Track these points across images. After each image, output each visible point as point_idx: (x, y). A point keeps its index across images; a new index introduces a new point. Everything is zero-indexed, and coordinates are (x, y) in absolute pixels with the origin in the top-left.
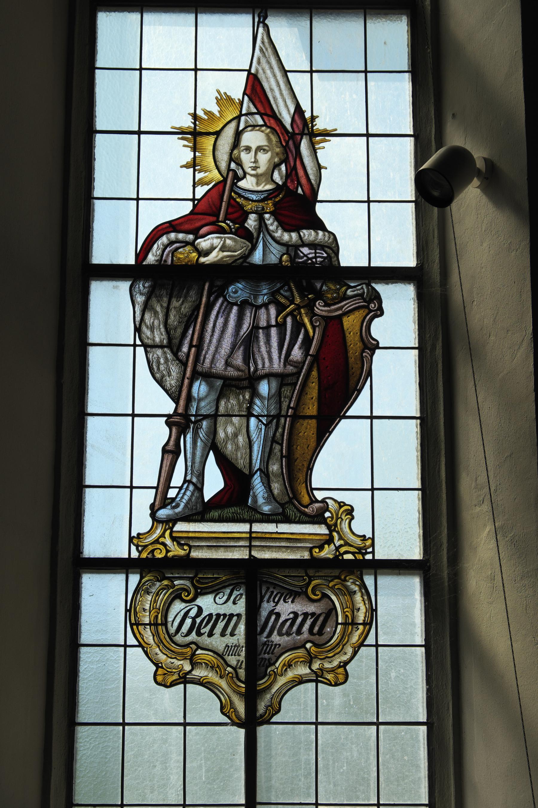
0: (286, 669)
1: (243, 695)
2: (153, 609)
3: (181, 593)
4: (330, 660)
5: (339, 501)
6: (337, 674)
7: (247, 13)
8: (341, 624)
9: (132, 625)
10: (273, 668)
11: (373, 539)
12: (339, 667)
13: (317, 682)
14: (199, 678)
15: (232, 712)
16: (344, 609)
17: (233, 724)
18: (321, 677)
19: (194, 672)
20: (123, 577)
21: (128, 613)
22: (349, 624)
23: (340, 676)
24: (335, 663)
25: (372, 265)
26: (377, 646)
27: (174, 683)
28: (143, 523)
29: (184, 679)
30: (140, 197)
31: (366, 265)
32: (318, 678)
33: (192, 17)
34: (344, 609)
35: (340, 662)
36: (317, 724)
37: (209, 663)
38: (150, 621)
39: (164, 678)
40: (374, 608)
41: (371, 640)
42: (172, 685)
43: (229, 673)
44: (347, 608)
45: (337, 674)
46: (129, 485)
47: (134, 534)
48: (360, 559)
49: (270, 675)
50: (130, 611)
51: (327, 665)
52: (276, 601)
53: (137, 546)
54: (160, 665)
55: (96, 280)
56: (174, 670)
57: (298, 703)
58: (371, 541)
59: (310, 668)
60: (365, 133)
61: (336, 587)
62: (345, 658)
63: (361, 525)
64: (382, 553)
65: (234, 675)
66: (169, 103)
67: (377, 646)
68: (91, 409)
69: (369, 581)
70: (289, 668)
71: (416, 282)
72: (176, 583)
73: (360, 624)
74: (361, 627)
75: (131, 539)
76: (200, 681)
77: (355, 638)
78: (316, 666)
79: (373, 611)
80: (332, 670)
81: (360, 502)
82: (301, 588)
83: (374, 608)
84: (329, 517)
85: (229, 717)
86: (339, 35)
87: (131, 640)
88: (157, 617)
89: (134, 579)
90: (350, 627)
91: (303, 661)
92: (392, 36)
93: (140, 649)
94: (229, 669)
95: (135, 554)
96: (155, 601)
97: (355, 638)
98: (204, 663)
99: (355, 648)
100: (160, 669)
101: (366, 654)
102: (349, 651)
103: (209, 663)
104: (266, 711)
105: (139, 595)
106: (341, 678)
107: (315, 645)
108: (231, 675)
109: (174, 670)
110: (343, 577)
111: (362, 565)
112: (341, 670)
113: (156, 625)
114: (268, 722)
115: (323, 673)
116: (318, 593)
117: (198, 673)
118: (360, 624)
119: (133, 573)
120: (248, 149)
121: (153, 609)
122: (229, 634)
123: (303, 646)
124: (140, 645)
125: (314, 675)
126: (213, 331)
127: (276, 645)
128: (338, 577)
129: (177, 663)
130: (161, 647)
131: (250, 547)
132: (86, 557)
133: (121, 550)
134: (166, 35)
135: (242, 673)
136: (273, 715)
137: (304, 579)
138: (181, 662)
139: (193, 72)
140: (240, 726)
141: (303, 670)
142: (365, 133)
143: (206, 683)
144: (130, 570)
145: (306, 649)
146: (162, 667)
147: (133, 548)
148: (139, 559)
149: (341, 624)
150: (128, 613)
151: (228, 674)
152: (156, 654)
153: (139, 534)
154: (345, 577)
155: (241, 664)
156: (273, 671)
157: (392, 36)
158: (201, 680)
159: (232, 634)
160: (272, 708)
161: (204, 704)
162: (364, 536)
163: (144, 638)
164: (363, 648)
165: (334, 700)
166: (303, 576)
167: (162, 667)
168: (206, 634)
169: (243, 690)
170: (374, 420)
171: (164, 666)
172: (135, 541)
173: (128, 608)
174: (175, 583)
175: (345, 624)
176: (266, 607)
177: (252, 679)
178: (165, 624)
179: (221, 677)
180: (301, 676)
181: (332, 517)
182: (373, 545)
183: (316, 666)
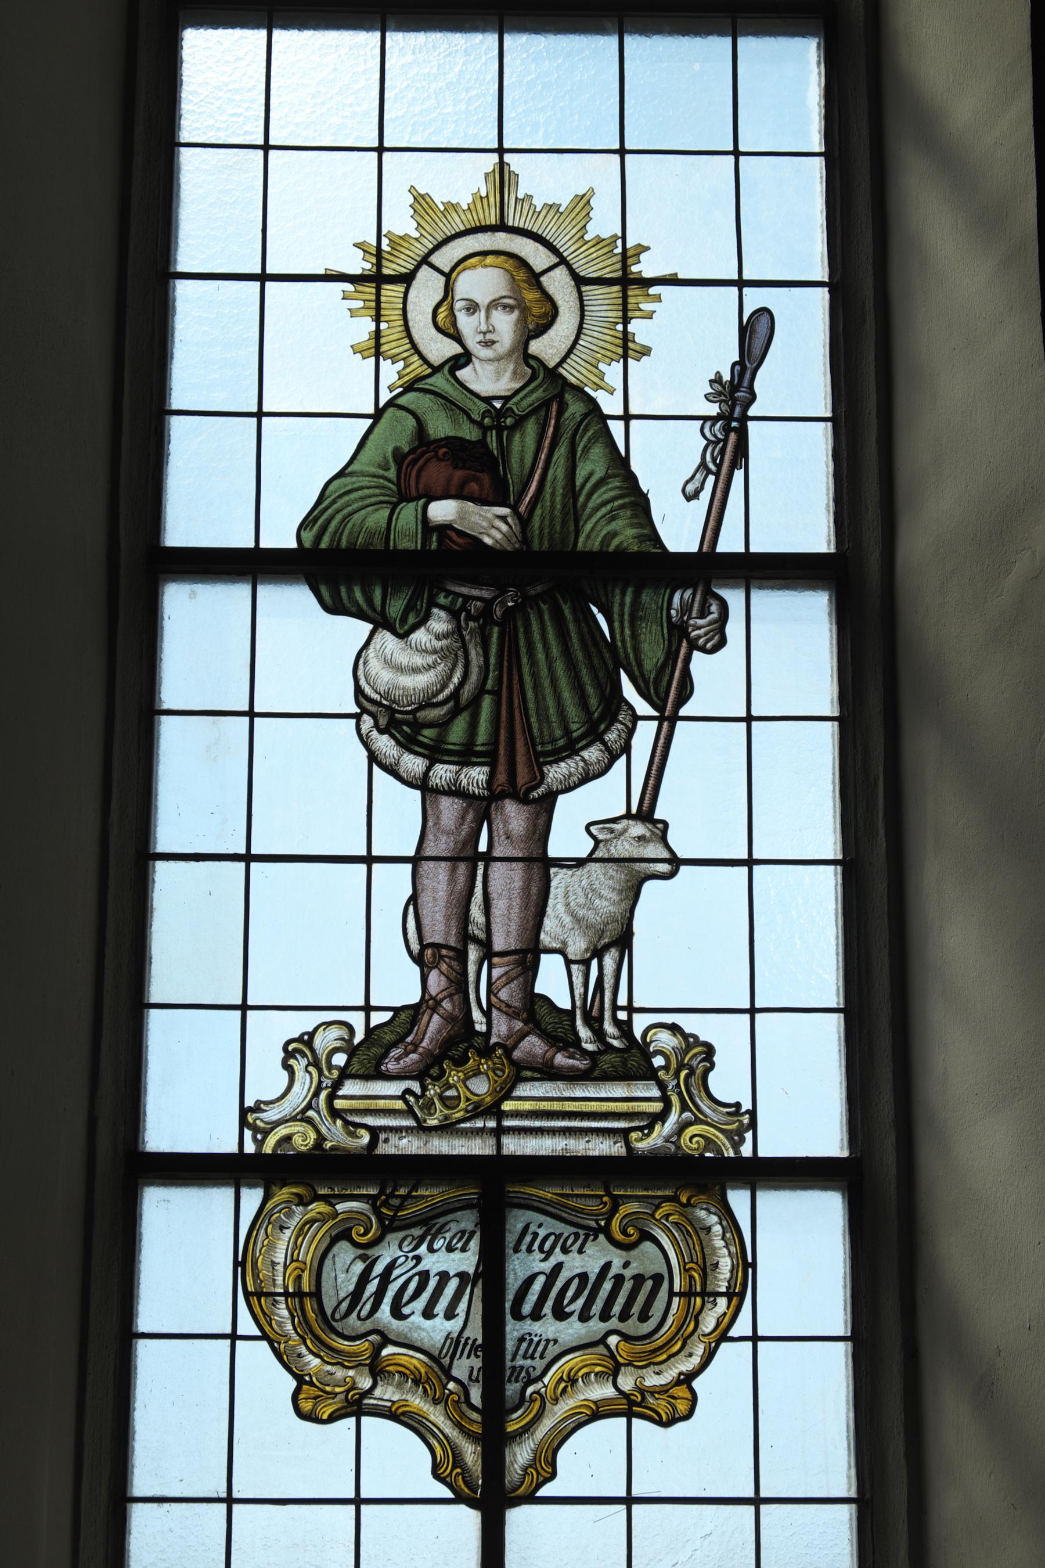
0: (566, 1387)
1: (479, 1439)
2: (292, 1261)
3: (351, 1228)
4: (657, 1368)
5: (297, 1036)
6: (674, 1398)
7: (721, 34)
8: (680, 1294)
9: (247, 1295)
10: (540, 1385)
11: (753, 1113)
12: (678, 1382)
13: (629, 1415)
14: (389, 1404)
15: (457, 1474)
16: (685, 1264)
17: (459, 1499)
18: (639, 1405)
19: (377, 1392)
20: (229, 1193)
21: (240, 1269)
22: (696, 1294)
23: (673, 1407)
24: (669, 1375)
25: (262, 545)
26: (755, 1338)
27: (337, 1414)
28: (267, 1080)
29: (356, 1407)
30: (265, 409)
31: (252, 545)
32: (630, 1407)
33: (611, 42)
34: (685, 1264)
35: (680, 1374)
36: (358, 1501)
37: (408, 1372)
38: (286, 1288)
39: (311, 1404)
40: (750, 1260)
41: (742, 1327)
42: (332, 1419)
43: (451, 1393)
44: (692, 1262)
45: (674, 1398)
46: (240, 1002)
47: (249, 1102)
48: (729, 1158)
49: (532, 1401)
50: (243, 1264)
51: (652, 1380)
52: (547, 1246)
53: (255, 1129)
54: (307, 1378)
55: (174, 581)
56: (338, 1390)
57: (590, 1458)
58: (744, 1120)
59: (615, 1385)
60: (736, 277)
61: (671, 1218)
62: (687, 1365)
63: (727, 1083)
64: (774, 1142)
65: (462, 1399)
66: (328, 218)
67: (755, 1338)
68: (164, 843)
69: (738, 1200)
70: (572, 1386)
71: (161, 576)
72: (340, 1207)
73: (721, 1294)
74: (722, 1302)
75: (244, 1112)
76: (390, 1411)
77: (708, 1323)
78: (627, 1382)
79: (746, 1266)
80: (664, 1390)
81: (726, 1036)
82: (597, 1221)
83: (750, 1260)
84: (661, 1068)
85: (449, 1486)
86: (678, 72)
87: (247, 1325)
88: (299, 1278)
89: (252, 1199)
90: (699, 1300)
91: (603, 1372)
92: (787, 78)
93: (264, 1344)
94: (451, 1385)
95: (250, 1148)
96: (297, 1246)
97: (708, 1323)
98: (398, 1372)
99: (710, 1343)
100: (305, 1387)
101: (732, 1357)
102: (699, 1350)
103: (408, 1372)
104: (524, 1475)
105: (263, 1231)
106: (682, 1407)
107: (626, 1337)
108: (456, 1398)
109: (338, 1390)
110: (684, 1200)
111: (721, 1171)
112: (681, 1391)
113: (299, 1294)
114: (531, 1499)
115: (644, 1398)
116: (631, 1230)
117: (387, 1393)
118: (721, 1294)
119: (252, 1186)
120: (472, 307)
121: (292, 1261)
122: (636, 1315)
123: (603, 1341)
124: (265, 1337)
125: (624, 1401)
126: (554, 682)
127: (548, 1341)
128: (675, 1199)
129: (340, 1373)
130: (309, 1342)
131: (499, 1132)
132: (152, 1151)
133: (222, 1138)
134: (325, 67)
135: (476, 1395)
136: (539, 1486)
137: (602, 1203)
138: (351, 1373)
139: (261, 153)
140: (472, 1503)
141: (604, 1391)
142: (736, 277)
143: (404, 1414)
144: (242, 1181)
145: (608, 1347)
146: (311, 1383)
147: (248, 1134)
148: (258, 1156)
149: (680, 1294)
150: (240, 1269)
151: (449, 1396)
152: (299, 1355)
153: (258, 1103)
154: (689, 1200)
155: (512, 1374)
156: (538, 1392)
157: (787, 78)
158: (393, 1409)
159: (450, 1315)
160: (536, 1470)
161: (397, 1457)
162: (738, 1105)
163: (273, 1322)
164: (724, 1346)
165: (665, 1456)
166: (601, 1197)
167: (311, 1383)
168: (576, 1314)
169: (477, 1429)
170: (253, 865)
171: (314, 1379)
172: (746, 1119)
173: (240, 1259)
174: (338, 1207)
175: (688, 1294)
176: (521, 1266)
177: (495, 1409)
178: (317, 1294)
179: (435, 1402)
180: (595, 1402)
181: (667, 1068)
182: (753, 1125)
183: (627, 1382)
